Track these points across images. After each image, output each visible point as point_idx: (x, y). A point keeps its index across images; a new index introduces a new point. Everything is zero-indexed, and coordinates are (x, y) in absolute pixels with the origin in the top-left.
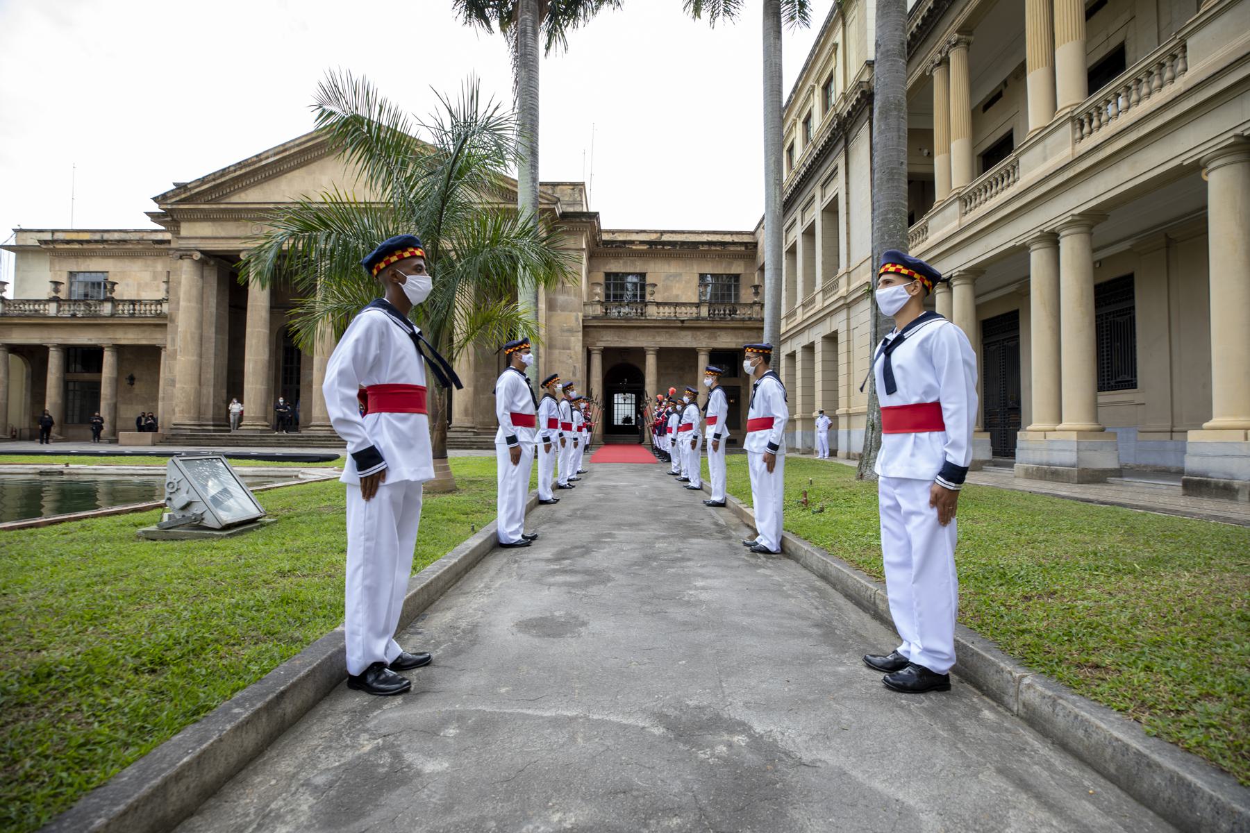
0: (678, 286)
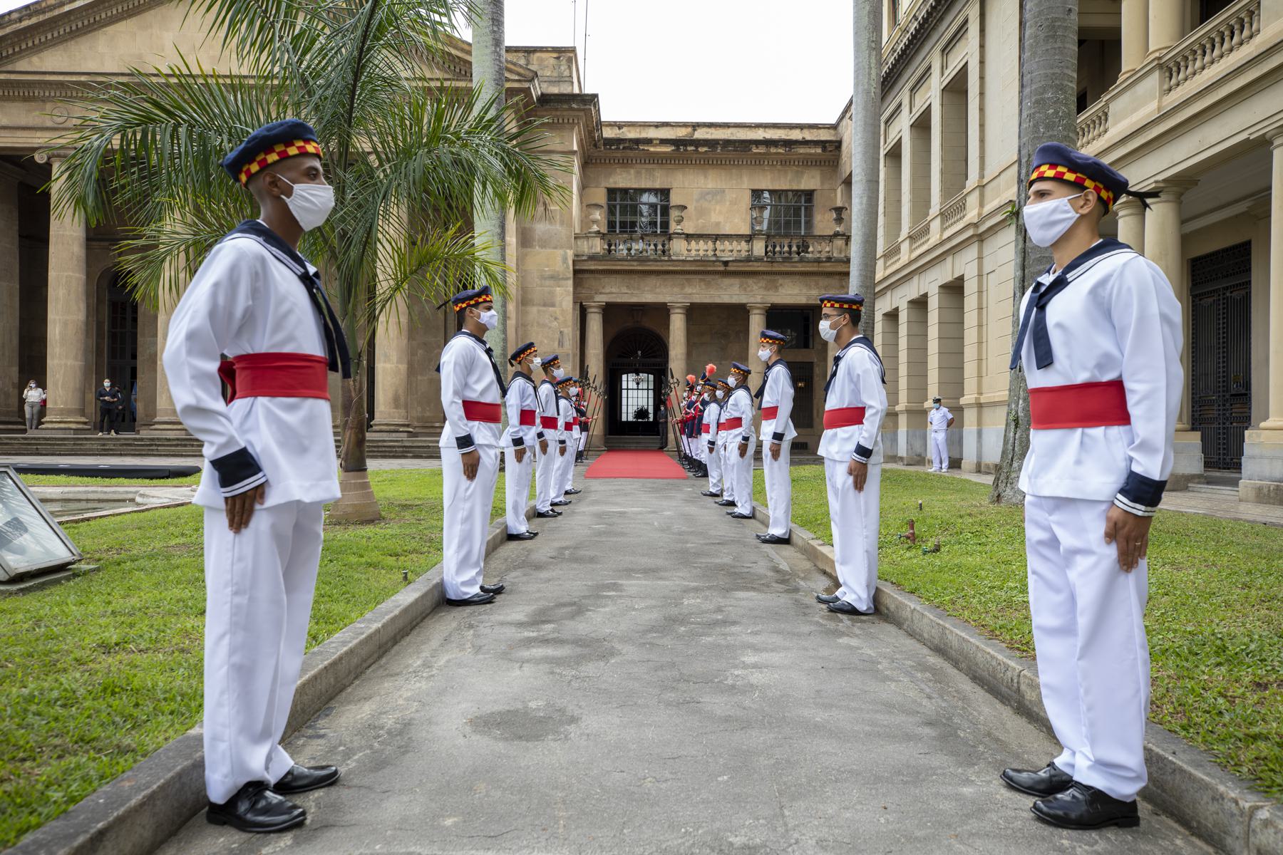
0: (718, 209)
